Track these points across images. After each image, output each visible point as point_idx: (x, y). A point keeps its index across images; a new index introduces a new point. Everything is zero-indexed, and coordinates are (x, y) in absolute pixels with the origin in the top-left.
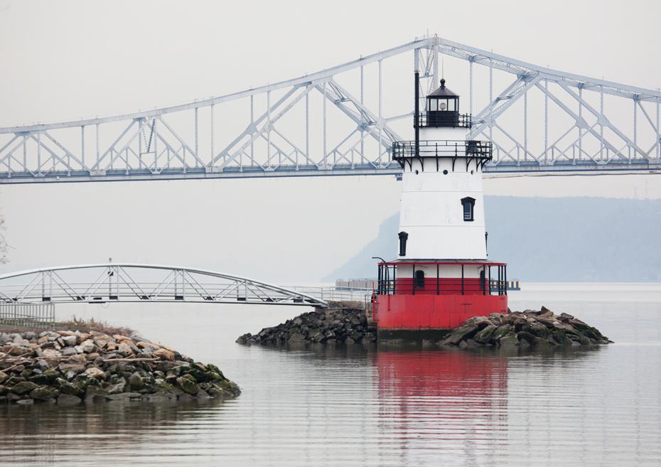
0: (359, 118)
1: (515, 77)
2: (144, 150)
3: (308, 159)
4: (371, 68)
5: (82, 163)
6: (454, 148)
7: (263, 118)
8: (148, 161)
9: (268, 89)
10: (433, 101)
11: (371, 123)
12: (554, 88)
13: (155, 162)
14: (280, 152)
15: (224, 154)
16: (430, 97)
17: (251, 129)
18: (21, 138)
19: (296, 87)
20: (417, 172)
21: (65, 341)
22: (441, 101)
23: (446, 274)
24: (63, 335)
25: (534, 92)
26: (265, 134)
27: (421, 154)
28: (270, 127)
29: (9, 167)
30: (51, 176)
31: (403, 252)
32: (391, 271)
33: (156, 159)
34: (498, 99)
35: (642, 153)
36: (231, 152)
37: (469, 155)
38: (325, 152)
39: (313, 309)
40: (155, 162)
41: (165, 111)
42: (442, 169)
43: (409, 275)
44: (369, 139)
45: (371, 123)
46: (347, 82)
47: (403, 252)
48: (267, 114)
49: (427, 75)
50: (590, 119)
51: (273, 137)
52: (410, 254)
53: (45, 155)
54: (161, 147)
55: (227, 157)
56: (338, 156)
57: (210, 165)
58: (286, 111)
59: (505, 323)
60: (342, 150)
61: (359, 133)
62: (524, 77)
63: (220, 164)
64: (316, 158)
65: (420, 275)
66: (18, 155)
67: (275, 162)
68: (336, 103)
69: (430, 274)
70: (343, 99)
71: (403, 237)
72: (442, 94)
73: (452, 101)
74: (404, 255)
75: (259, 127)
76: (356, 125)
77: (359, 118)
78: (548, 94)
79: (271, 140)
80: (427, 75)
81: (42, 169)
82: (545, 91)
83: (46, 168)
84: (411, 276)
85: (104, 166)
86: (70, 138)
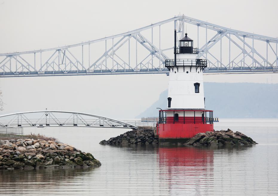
0: (151, 49)
1: (217, 32)
2: (61, 63)
3: (129, 67)
4: (156, 28)
5: (34, 68)
6: (191, 62)
7: (110, 49)
8: (62, 68)
9: (113, 37)
10: (182, 43)
11: (156, 52)
12: (233, 37)
13: (65, 68)
14: (118, 64)
15: (94, 64)
16: (181, 41)
17: (106, 54)
18: (9, 58)
19: (125, 37)
20: (187, 72)
21: (27, 143)
22: (185, 42)
23: (188, 115)
24: (26, 141)
25: (224, 39)
26: (112, 56)
27: (177, 65)
28: (114, 53)
29: (4, 70)
30: (22, 74)
31: (169, 106)
32: (164, 114)
33: (66, 67)
34: (210, 42)
35: (270, 64)
36: (97, 64)
37: (197, 65)
38: (137, 64)
39: (132, 130)
40: (65, 68)
41: (69, 46)
42: (186, 71)
43: (172, 115)
44: (155, 58)
45: (156, 52)
46: (146, 34)
47: (169, 106)
48: (112, 48)
49: (179, 31)
50: (248, 50)
51: (115, 57)
52: (173, 107)
53: (19, 65)
54: (68, 62)
55: (95, 66)
56: (142, 66)
57: (88, 69)
58: (120, 46)
59: (212, 135)
60: (144, 63)
61: (151, 56)
62: (220, 32)
63: (92, 69)
64: (133, 67)
65: (177, 115)
66: (8, 65)
67: (116, 68)
68: (141, 43)
69: (181, 115)
70: (144, 42)
71: (170, 99)
72: (186, 39)
73: (190, 43)
74: (170, 107)
75: (109, 53)
76: (150, 53)
77: (151, 49)
78: (230, 40)
79: (114, 59)
80: (179, 31)
81: (18, 71)
82: (229, 38)
83: (19, 71)
84: (173, 116)
85: (44, 69)
86: (29, 58)
